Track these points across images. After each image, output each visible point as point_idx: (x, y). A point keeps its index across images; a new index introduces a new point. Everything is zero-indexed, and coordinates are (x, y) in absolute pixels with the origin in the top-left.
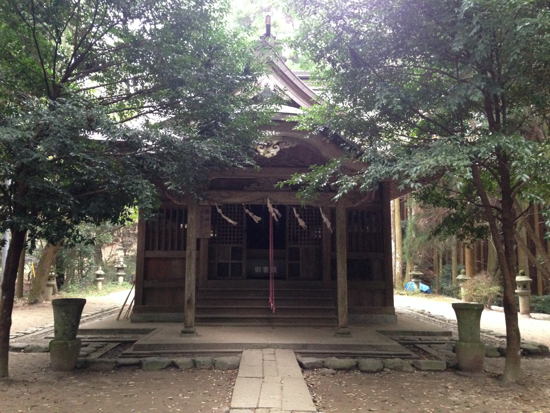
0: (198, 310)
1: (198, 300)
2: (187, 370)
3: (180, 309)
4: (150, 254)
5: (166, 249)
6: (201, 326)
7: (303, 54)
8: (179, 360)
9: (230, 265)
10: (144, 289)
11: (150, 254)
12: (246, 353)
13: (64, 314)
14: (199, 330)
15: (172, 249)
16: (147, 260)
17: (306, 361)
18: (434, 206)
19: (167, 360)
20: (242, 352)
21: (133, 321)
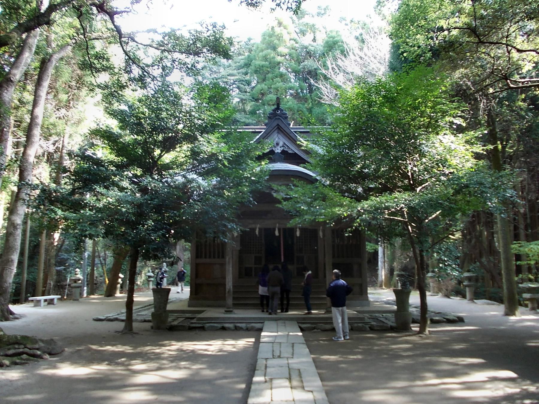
0: (234, 298)
1: (234, 292)
2: (233, 330)
3: (224, 299)
4: (200, 261)
5: (210, 257)
6: (237, 309)
7: (460, 282)
8: (226, 325)
9: (253, 269)
10: (196, 284)
11: (200, 261)
12: (266, 322)
13: (159, 297)
14: (235, 311)
15: (214, 257)
16: (197, 265)
17: (303, 326)
18: (199, 57)
19: (219, 326)
20: (263, 323)
21: (189, 306)
